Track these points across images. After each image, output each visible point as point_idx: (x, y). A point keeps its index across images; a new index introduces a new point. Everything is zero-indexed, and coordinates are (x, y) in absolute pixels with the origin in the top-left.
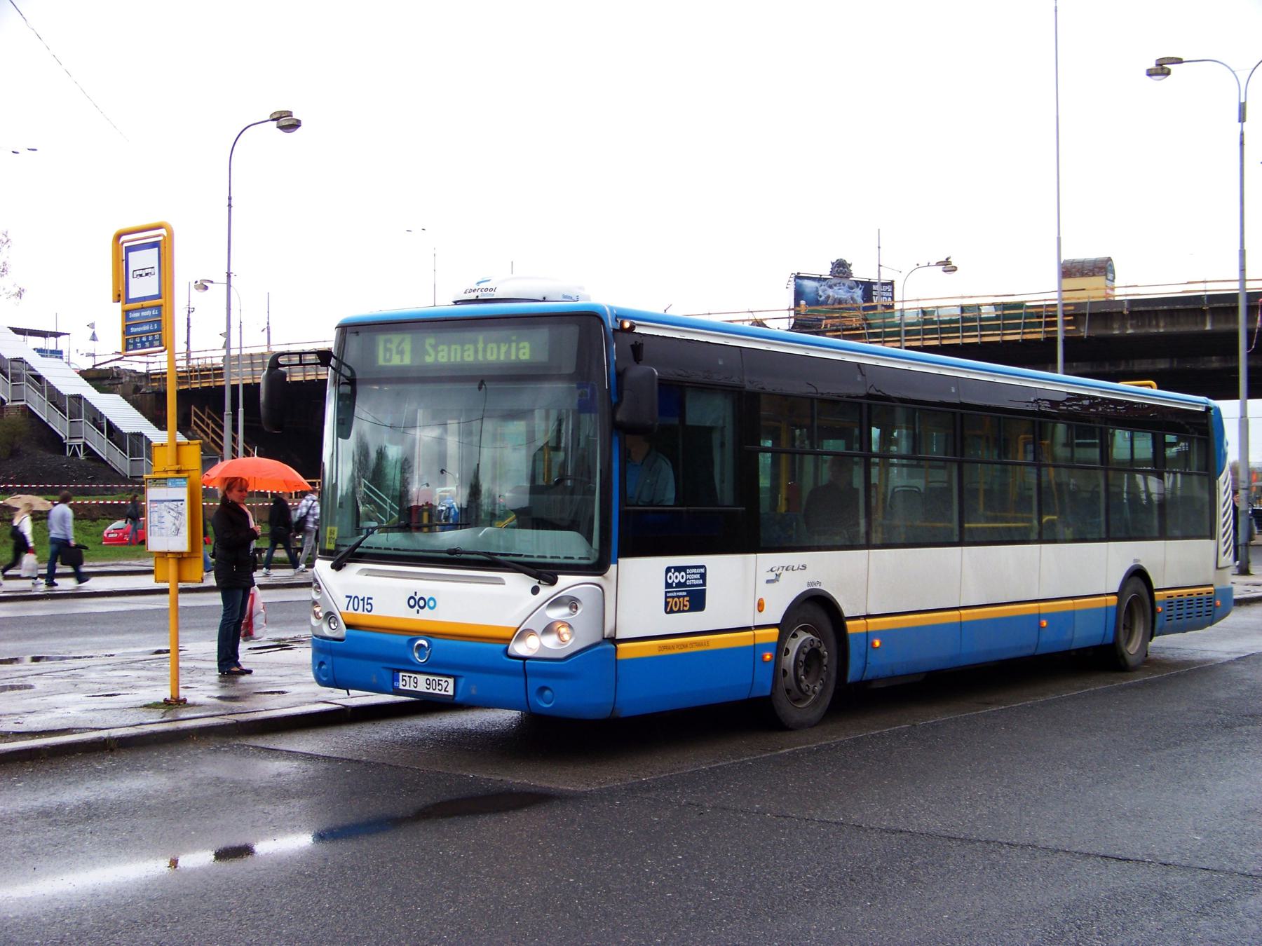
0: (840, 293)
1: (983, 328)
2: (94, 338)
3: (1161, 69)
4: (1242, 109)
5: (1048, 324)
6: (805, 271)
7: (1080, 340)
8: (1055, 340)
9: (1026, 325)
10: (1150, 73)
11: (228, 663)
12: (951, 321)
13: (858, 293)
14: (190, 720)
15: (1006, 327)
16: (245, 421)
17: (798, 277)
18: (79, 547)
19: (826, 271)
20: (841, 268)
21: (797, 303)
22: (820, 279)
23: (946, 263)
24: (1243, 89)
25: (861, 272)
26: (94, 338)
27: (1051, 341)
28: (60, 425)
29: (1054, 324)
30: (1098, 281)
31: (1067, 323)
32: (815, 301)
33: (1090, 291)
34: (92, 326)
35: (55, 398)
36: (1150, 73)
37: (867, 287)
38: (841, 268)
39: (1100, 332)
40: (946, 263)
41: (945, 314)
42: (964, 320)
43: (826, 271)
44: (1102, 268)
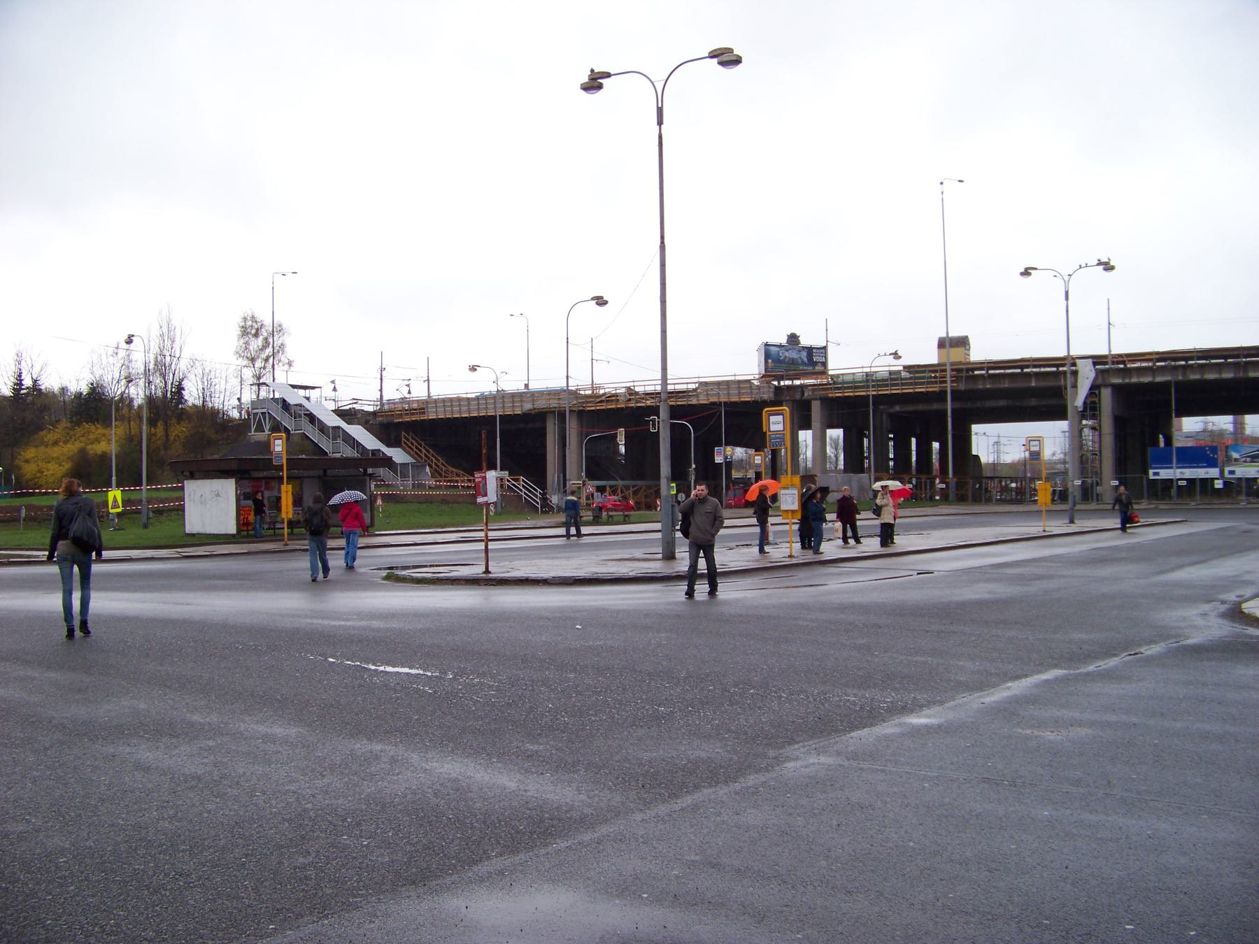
0: (793, 354)
1: (903, 384)
2: (335, 390)
3: (1026, 273)
4: (1067, 293)
5: (941, 382)
6: (771, 341)
7: (960, 392)
8: (945, 392)
9: (928, 383)
10: (1022, 274)
11: (762, 551)
12: (883, 380)
13: (804, 354)
14: (794, 561)
15: (916, 384)
16: (544, 446)
17: (767, 345)
18: (1099, 498)
19: (784, 341)
20: (793, 338)
21: (766, 362)
22: (780, 346)
23: (896, 353)
24: (1067, 284)
25: (805, 341)
26: (335, 390)
27: (944, 392)
28: (326, 445)
29: (945, 382)
30: (960, 350)
31: (952, 382)
32: (778, 361)
33: (956, 355)
34: (333, 382)
35: (323, 428)
36: (1022, 274)
37: (810, 350)
38: (793, 338)
39: (971, 386)
40: (896, 353)
41: (879, 376)
42: (892, 379)
43: (784, 341)
44: (962, 342)
